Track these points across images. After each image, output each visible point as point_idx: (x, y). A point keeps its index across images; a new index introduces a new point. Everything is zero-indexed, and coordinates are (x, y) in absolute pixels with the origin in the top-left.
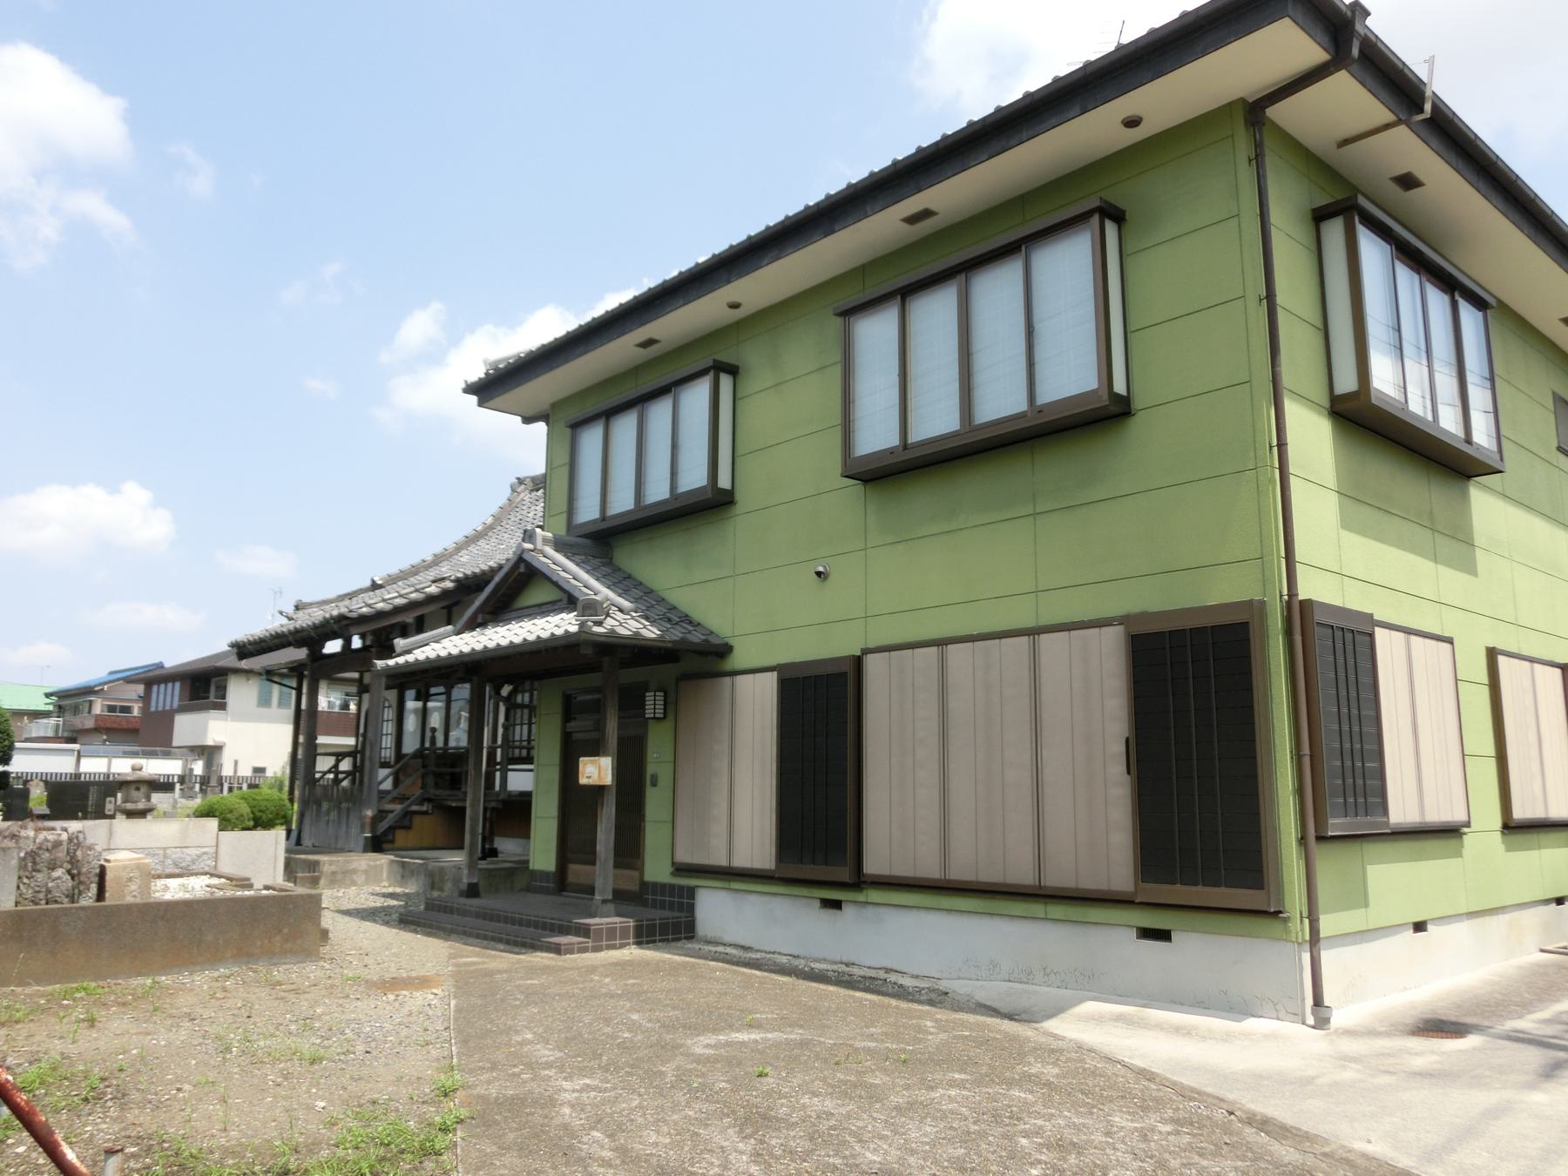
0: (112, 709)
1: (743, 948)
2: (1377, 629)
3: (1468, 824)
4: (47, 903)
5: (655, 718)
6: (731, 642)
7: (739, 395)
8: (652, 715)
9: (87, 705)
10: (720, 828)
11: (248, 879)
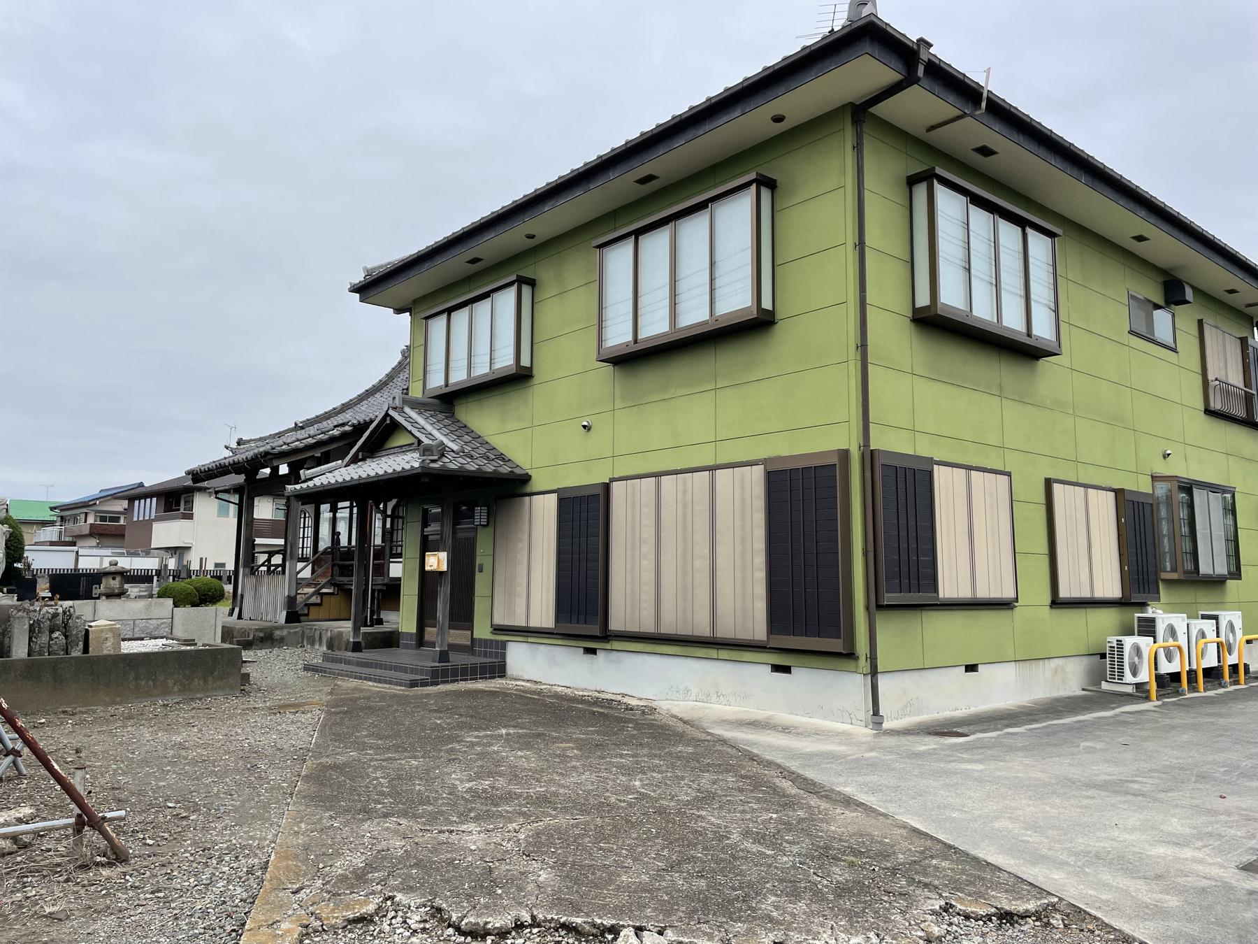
0: (103, 519)
1: (536, 682)
2: (936, 467)
3: (1016, 600)
4: (49, 655)
5: (480, 525)
6: (530, 472)
7: (535, 301)
8: (479, 523)
9: (83, 516)
10: (520, 602)
11: (194, 640)
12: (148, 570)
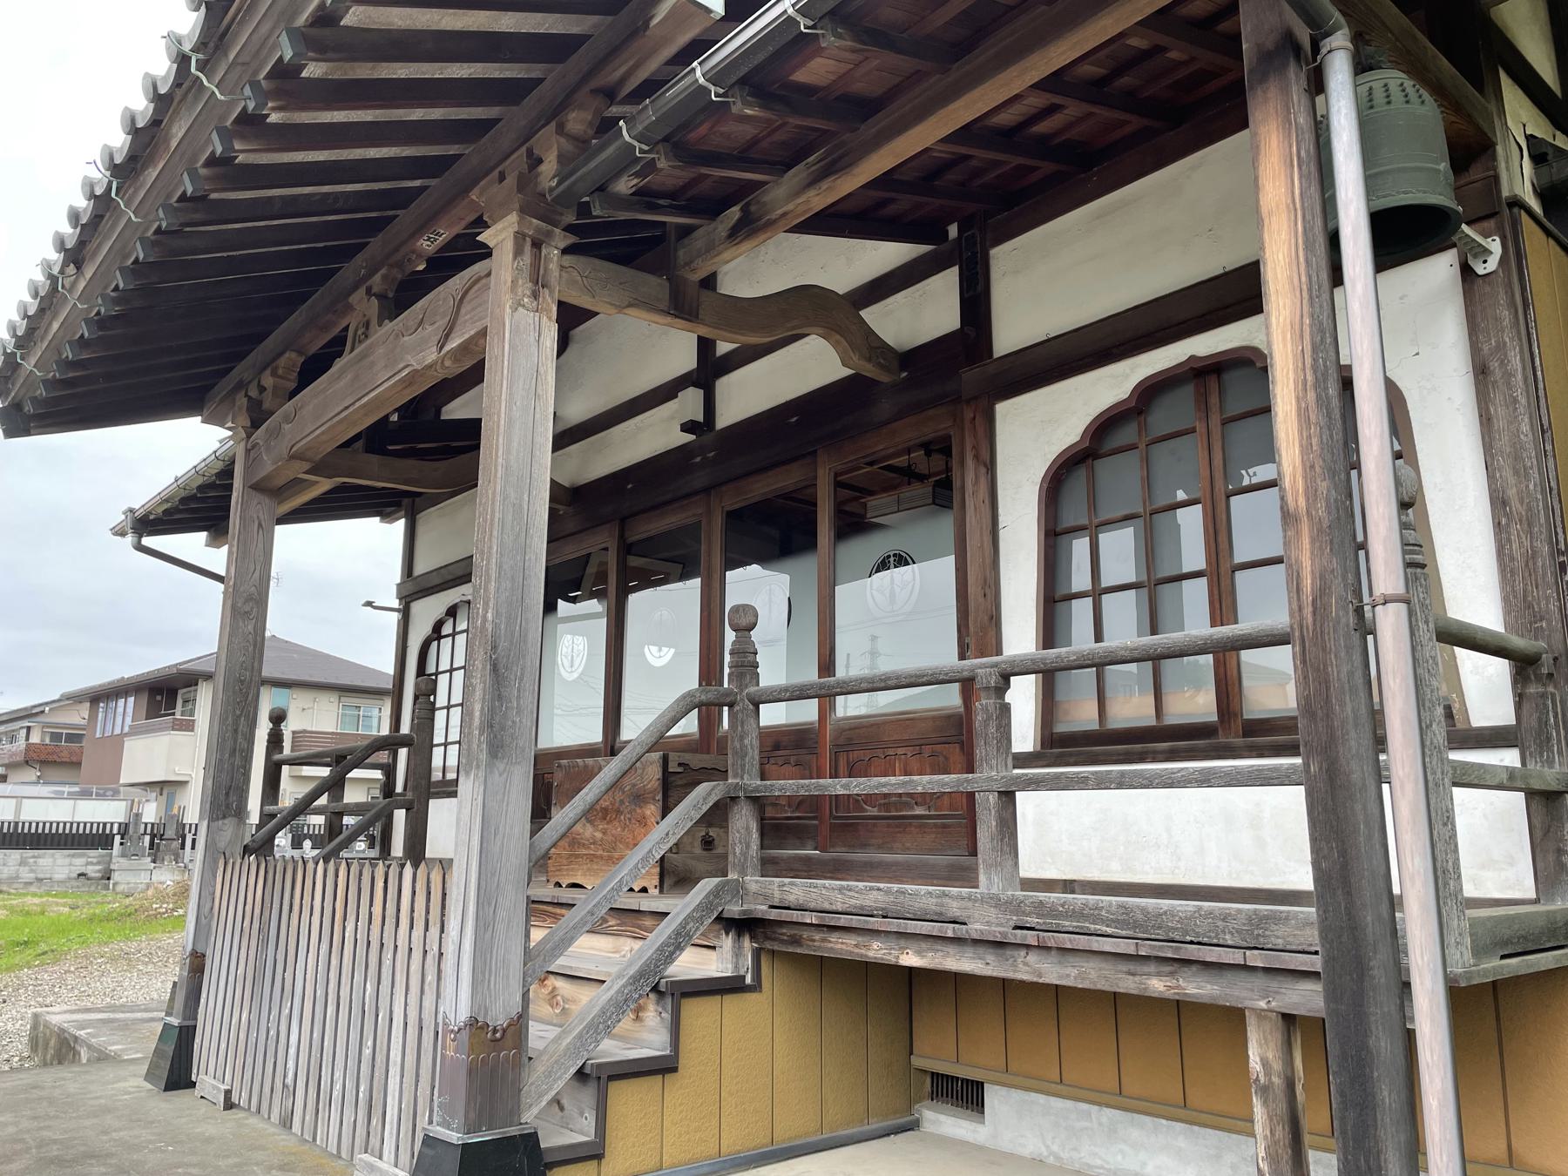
0: (56, 737)
9: (23, 732)
12: (105, 824)
